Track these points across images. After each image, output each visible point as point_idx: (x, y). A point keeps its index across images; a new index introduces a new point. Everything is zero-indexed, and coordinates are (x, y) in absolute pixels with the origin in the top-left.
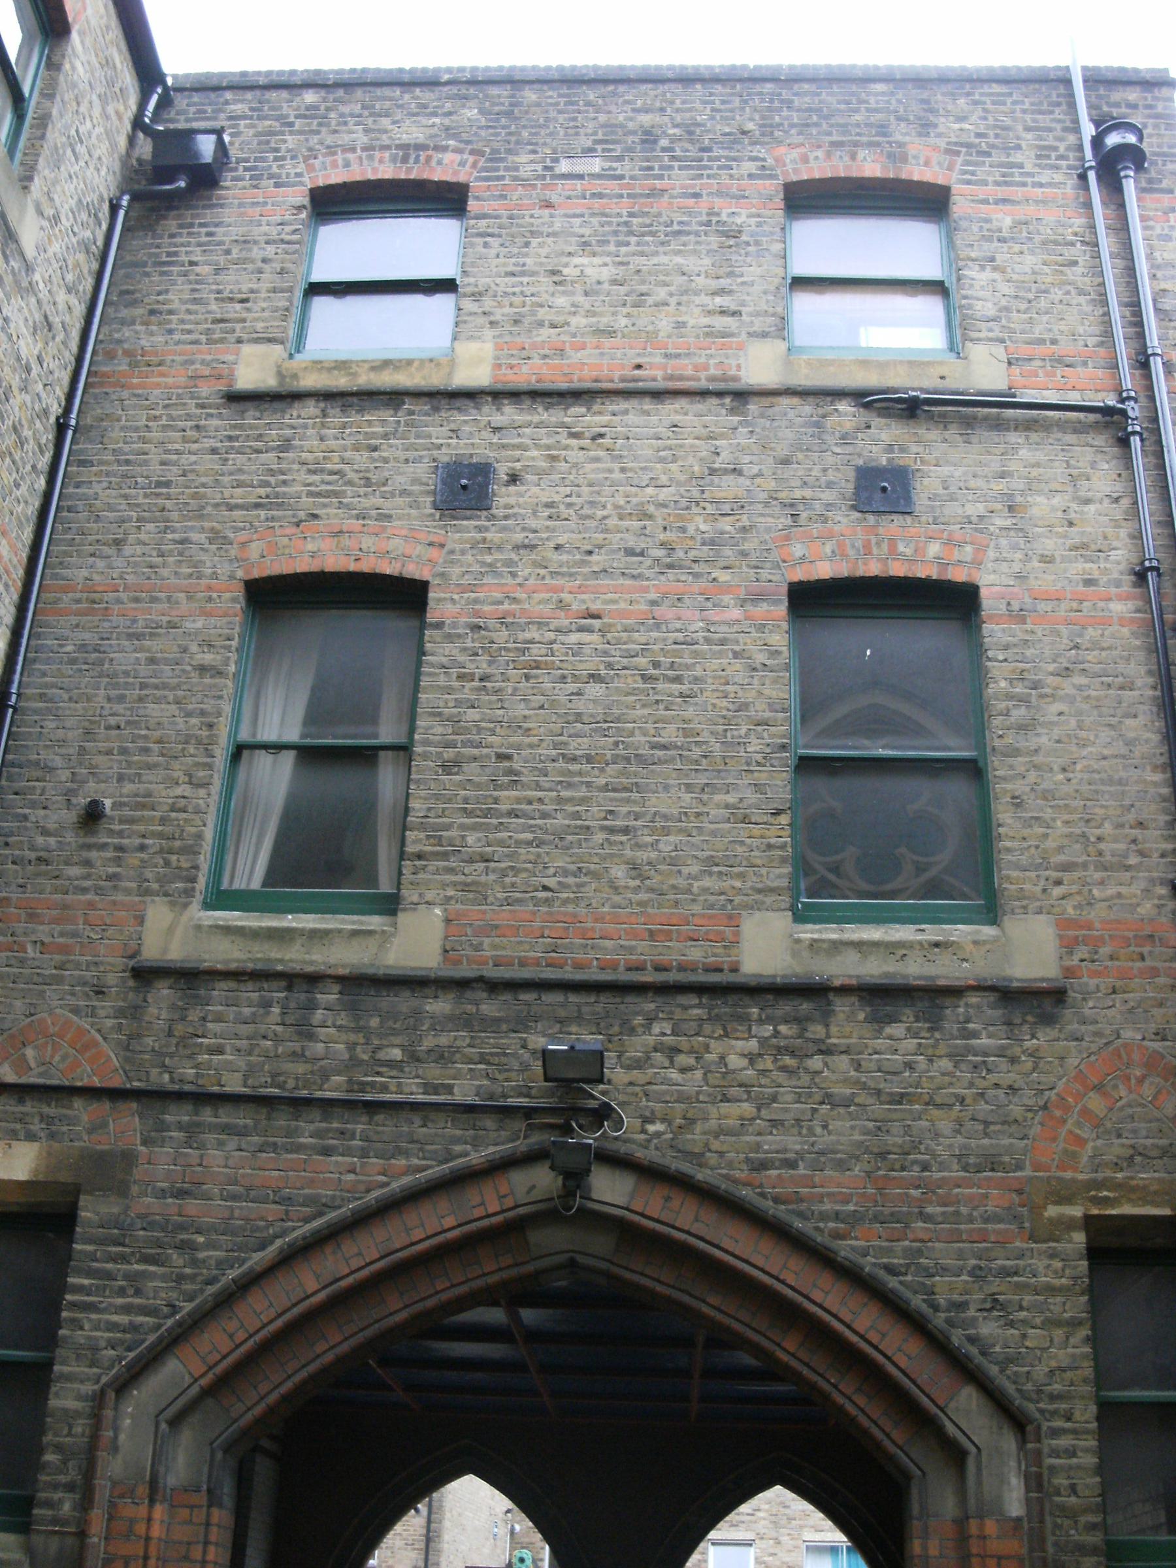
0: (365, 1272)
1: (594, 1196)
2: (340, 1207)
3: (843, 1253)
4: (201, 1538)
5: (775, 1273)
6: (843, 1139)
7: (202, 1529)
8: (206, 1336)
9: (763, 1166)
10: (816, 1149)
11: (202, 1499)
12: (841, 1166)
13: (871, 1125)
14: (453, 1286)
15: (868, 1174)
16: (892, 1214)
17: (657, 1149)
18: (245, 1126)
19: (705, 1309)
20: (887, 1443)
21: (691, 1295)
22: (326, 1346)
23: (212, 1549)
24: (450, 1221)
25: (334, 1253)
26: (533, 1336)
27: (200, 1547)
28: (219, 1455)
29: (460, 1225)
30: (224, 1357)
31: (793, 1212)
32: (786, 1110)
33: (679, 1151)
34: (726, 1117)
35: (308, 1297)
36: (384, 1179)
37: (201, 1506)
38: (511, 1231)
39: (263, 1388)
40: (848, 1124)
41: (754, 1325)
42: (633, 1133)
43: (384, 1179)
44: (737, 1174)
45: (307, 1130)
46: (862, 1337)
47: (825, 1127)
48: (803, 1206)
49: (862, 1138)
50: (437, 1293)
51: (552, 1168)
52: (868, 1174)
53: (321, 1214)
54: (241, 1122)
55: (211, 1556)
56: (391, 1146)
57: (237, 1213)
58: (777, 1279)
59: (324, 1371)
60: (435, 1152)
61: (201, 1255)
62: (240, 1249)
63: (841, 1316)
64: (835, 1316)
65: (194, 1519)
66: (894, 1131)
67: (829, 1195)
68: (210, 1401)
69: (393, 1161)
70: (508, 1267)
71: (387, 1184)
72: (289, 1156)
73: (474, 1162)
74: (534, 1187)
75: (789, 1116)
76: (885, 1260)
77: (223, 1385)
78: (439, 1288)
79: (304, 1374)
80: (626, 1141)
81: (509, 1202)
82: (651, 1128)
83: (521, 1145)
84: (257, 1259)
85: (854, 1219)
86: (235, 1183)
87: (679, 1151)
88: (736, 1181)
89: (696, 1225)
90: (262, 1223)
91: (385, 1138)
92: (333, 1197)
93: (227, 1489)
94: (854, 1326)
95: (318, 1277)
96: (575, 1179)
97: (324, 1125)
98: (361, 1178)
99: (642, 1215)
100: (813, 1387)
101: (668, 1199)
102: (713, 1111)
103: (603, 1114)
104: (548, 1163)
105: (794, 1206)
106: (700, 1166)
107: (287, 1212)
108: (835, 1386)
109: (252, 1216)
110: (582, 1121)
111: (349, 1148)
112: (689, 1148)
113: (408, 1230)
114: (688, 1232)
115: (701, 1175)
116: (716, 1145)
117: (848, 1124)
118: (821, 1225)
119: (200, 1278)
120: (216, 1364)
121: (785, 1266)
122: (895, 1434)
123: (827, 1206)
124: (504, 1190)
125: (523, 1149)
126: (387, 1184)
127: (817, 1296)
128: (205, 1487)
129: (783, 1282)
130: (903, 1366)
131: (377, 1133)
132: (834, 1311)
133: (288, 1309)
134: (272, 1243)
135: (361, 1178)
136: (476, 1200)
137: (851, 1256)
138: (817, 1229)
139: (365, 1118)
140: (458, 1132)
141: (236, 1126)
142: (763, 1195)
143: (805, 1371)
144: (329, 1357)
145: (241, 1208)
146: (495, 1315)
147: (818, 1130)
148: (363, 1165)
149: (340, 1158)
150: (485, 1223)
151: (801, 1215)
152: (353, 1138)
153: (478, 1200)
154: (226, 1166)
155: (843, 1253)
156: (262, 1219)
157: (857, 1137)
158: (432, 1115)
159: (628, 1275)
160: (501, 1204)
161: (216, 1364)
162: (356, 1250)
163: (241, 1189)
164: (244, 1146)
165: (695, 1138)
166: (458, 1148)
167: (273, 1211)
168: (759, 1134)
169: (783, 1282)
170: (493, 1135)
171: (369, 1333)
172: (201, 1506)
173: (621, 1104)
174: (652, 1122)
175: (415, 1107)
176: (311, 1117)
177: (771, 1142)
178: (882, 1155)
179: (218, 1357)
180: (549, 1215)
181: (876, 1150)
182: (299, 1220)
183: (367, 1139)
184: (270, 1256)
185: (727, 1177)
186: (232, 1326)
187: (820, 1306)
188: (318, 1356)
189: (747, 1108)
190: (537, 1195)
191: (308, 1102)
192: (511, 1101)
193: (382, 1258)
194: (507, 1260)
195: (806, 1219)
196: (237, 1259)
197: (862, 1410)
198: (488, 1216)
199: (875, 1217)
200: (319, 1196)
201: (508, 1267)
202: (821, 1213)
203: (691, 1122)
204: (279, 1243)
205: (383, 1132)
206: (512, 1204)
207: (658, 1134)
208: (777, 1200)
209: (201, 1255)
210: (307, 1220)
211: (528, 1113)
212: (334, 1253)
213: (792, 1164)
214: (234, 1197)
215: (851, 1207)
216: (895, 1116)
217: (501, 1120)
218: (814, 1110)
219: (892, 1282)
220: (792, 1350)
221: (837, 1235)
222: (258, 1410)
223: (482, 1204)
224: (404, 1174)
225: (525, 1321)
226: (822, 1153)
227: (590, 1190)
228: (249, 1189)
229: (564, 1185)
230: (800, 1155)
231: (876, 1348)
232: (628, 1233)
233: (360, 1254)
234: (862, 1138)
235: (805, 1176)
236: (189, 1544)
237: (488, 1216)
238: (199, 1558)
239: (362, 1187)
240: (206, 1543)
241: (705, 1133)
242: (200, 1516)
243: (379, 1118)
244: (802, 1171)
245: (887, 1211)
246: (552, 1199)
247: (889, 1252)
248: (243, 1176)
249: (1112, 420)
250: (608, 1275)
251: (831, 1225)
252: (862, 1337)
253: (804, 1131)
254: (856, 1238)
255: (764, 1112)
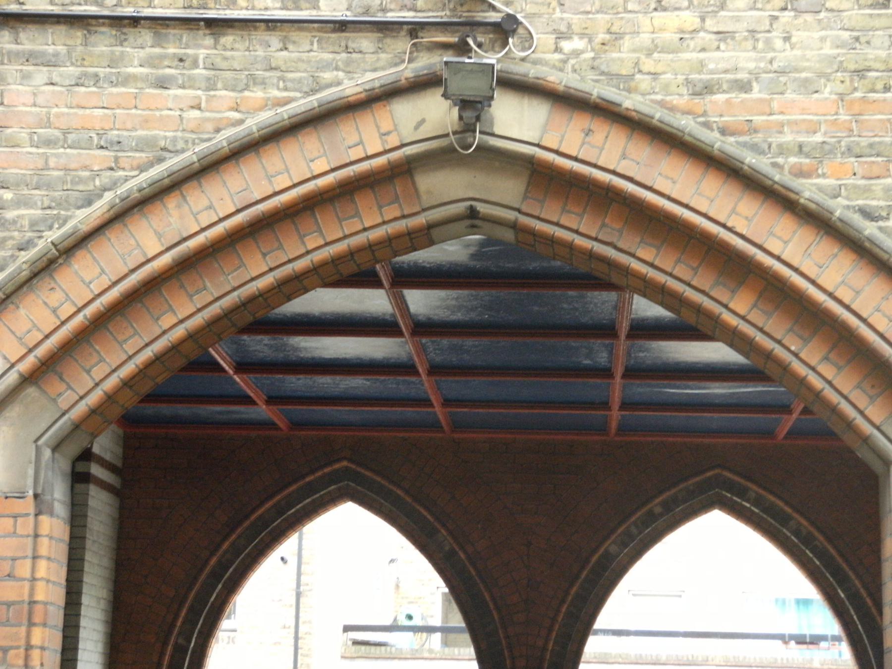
0: (219, 229)
1: (497, 131)
2: (183, 151)
3: (837, 213)
4: (30, 553)
5: (722, 219)
6: (809, 54)
7: (30, 540)
8: (22, 311)
9: (708, 89)
10: (775, 66)
11: (29, 505)
12: (807, 87)
13: (846, 35)
14: (327, 244)
15: (841, 96)
16: (871, 146)
17: (575, 71)
18: (56, 55)
19: (635, 265)
20: (860, 421)
21: (616, 248)
22: (175, 320)
23: (42, 565)
24: (321, 165)
25: (179, 206)
26: (423, 328)
27: (28, 562)
28: (47, 453)
29: (333, 170)
30: (47, 337)
31: (744, 145)
32: (738, 19)
33: (602, 73)
34: (662, 30)
35: (149, 261)
36: (236, 115)
37: (27, 515)
38: (394, 176)
39: (98, 372)
40: (817, 35)
41: (694, 283)
42: (545, 54)
43: (236, 115)
44: (675, 100)
45: (138, 51)
46: (831, 295)
47: (787, 39)
48: (758, 138)
49: (836, 51)
50: (308, 252)
51: (445, 96)
52: (841, 96)
53: (160, 160)
54: (51, 49)
55: (41, 572)
56: (243, 76)
57: (52, 163)
58: (724, 226)
59: (174, 349)
60: (300, 81)
61: (10, 215)
62: (59, 205)
63: (804, 269)
64: (796, 270)
65: (19, 531)
66: (876, 42)
67: (789, 123)
68: (31, 391)
69: (247, 93)
70: (396, 219)
71: (242, 122)
72: (115, 90)
73: (348, 92)
74: (423, 121)
75: (741, 27)
76: (860, 202)
77: (46, 369)
78: (310, 246)
79: (148, 354)
80: (535, 63)
81: (393, 141)
82: (567, 46)
83: (407, 71)
84: (83, 218)
85: (824, 151)
86: (49, 125)
87: (602, 73)
88: (672, 109)
89: (624, 163)
90: (86, 174)
91: (236, 66)
92: (174, 140)
93: (59, 493)
94: (820, 281)
95: (159, 236)
96: (472, 108)
97: (157, 50)
98: (208, 114)
99: (557, 152)
100: (769, 356)
101: (588, 132)
102: (644, 22)
103: (504, 30)
104: (441, 90)
105: (746, 138)
106: (629, 91)
107: (116, 159)
108: (796, 355)
109: (73, 166)
110: (480, 39)
111: (191, 78)
112: (614, 69)
113: (269, 178)
114: (614, 172)
115: (629, 103)
116: (648, 65)
117: (817, 35)
118: (780, 160)
119: (10, 243)
120: (36, 346)
121: (733, 211)
122: (870, 412)
123: (788, 137)
124: (386, 126)
125: (409, 74)
126: (242, 122)
127: (774, 246)
128: (31, 493)
129: (730, 229)
130: (881, 328)
131: (226, 59)
132: (795, 263)
133: (126, 276)
134: (100, 196)
135: (208, 114)
136: (353, 139)
137: (819, 197)
138: (775, 165)
139: (209, 41)
140: (327, 56)
141: (43, 54)
142: (707, 125)
143: (759, 338)
144: (179, 333)
145: (57, 156)
146: (374, 301)
147: (779, 44)
148: (210, 99)
149: (180, 92)
150: (365, 166)
151: (755, 148)
152: (195, 64)
153: (354, 139)
154: (35, 105)
155: (807, 194)
156: (85, 168)
157: (828, 50)
158: (295, 35)
159: (539, 226)
160: (384, 142)
161: (36, 346)
162: (206, 203)
163: (57, 133)
164: (56, 79)
165: (621, 58)
166: (327, 76)
167: (100, 158)
168: (703, 50)
169: (730, 229)
170: (371, 58)
171: (226, 302)
172: (27, 515)
173: (530, 16)
174: (569, 38)
175: (271, 24)
176: (140, 41)
177: (719, 60)
178: (860, 73)
179: (40, 337)
180: (441, 156)
181: (852, 67)
182: (132, 169)
183: (213, 67)
184: (99, 213)
185: (662, 104)
186: (55, 298)
187: (778, 258)
188: (164, 332)
189: (689, 19)
190: (426, 131)
191: (135, 21)
192: (391, 16)
193: (238, 211)
194: (392, 212)
195: (762, 153)
196: (57, 217)
197: (830, 383)
198: (368, 158)
199: (849, 149)
200: (155, 138)
201: (396, 219)
202: (780, 146)
203: (618, 36)
204: (108, 196)
205: (233, 58)
206: (397, 143)
207: (576, 53)
208: (724, 131)
209: (10, 215)
210: (142, 169)
211: (415, 29)
212: (179, 206)
213: (744, 87)
214: (49, 143)
215: (818, 138)
216: (877, 23)
217: (380, 40)
218: (776, 18)
219: (869, 229)
220: (742, 312)
221: (800, 173)
222: (94, 399)
223: (361, 143)
224: (263, 108)
225: (413, 308)
226: (782, 72)
227: (492, 124)
228: (66, 132)
229: (461, 118)
230: (756, 75)
231: (847, 307)
232: (545, 178)
233: (210, 207)
234: (836, 51)
235: (761, 100)
236: (14, 559)
237: (368, 158)
238: (28, 575)
239: (210, 127)
240: (35, 558)
241: (634, 51)
242: (26, 526)
243: (228, 39)
244: (756, 93)
245: (864, 142)
246: (447, 135)
247: (866, 191)
248: (58, 116)
249: (15, 533)
250: (514, 226)
251: (793, 160)
252: (831, 295)
253: (760, 45)
254: (824, 175)
255: (709, 23)
